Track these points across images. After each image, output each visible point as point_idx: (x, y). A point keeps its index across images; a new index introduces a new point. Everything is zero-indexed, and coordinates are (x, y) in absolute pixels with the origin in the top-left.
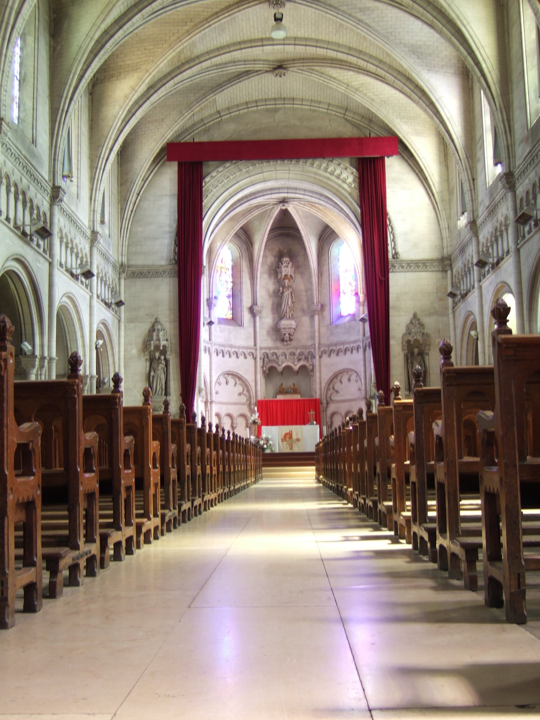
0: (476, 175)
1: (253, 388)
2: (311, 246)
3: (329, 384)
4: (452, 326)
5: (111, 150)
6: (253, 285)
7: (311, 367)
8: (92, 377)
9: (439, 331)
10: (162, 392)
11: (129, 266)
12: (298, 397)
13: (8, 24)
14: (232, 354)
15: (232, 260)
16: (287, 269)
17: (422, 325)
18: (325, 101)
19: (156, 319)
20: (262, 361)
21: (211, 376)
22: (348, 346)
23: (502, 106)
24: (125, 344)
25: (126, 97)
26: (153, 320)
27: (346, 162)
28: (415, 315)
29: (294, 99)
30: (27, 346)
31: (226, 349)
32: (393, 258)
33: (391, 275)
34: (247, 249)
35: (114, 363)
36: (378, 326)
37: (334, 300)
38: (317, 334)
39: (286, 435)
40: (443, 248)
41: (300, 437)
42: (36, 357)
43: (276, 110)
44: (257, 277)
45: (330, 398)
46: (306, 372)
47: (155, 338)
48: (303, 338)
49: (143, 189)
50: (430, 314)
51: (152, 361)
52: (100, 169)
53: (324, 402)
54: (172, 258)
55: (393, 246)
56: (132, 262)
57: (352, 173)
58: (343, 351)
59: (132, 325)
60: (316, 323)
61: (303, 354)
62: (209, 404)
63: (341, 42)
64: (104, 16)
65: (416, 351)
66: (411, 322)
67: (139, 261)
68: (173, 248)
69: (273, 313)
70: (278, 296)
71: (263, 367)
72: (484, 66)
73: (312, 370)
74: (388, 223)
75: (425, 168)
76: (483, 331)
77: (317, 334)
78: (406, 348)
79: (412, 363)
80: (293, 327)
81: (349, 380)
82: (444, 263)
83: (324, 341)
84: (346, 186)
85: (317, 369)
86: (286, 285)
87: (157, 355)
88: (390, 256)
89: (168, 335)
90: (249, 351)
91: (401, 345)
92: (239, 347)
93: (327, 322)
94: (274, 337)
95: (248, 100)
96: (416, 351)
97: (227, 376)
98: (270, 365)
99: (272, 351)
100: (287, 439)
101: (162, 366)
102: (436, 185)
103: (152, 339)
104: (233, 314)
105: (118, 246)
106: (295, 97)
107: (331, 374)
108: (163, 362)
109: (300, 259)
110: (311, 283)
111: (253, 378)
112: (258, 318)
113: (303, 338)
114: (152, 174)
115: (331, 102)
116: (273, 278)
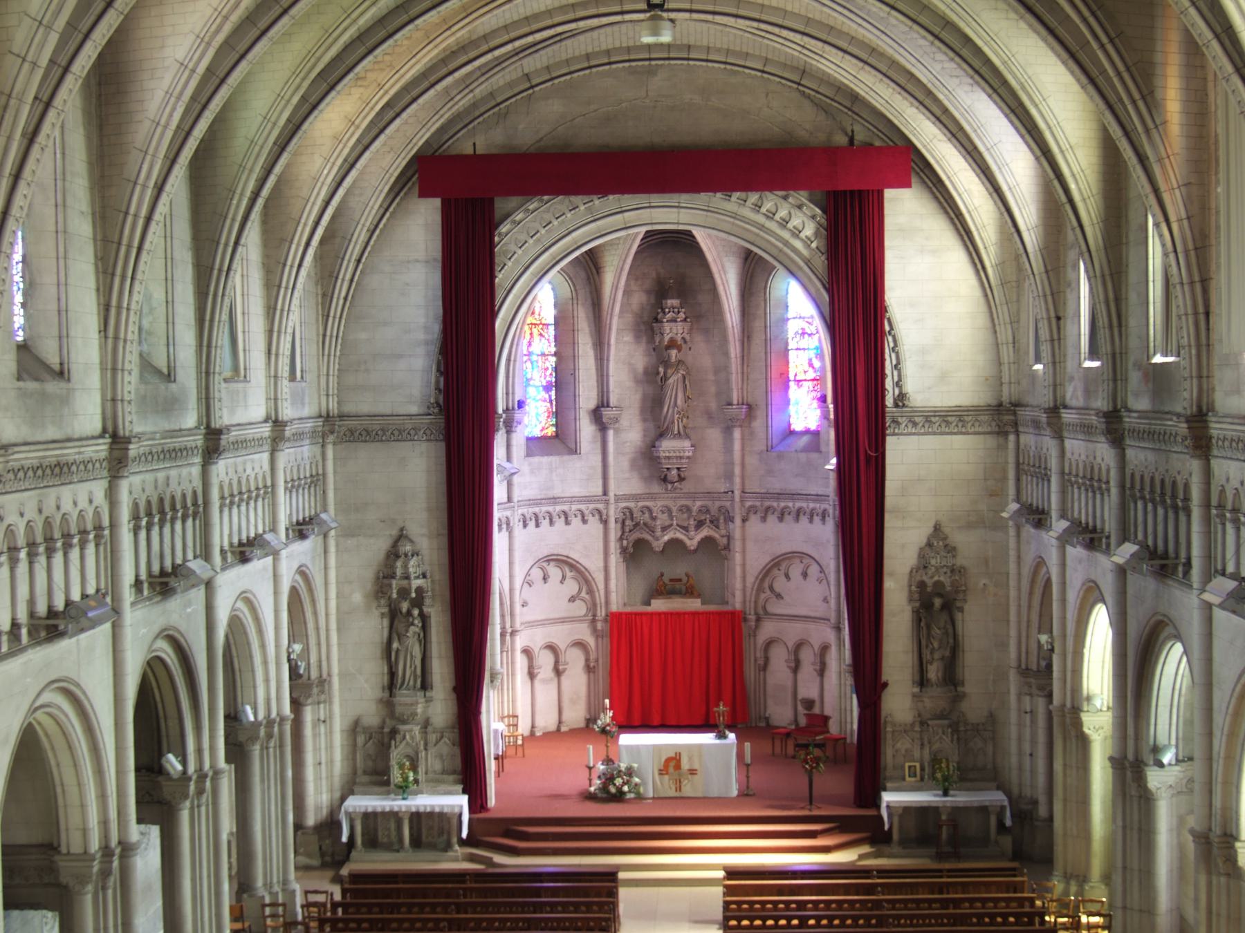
0: (1065, 310)
1: (601, 586)
2: (728, 280)
3: (762, 580)
4: (1012, 553)
5: (308, 244)
6: (602, 359)
7: (725, 541)
8: (282, 719)
9: (986, 562)
10: (415, 681)
11: (342, 416)
12: (694, 605)
13: (129, 246)
14: (555, 518)
15: (556, 306)
16: (673, 329)
17: (951, 550)
18: (757, 53)
19: (402, 530)
20: (619, 525)
21: (511, 576)
22: (804, 505)
23: (1107, 272)
24: (337, 582)
25: (338, 139)
26: (395, 532)
27: (802, 196)
28: (937, 528)
29: (689, 46)
30: (172, 763)
31: (544, 509)
32: (896, 405)
33: (890, 441)
34: (589, 279)
35: (317, 629)
36: (860, 556)
37: (776, 397)
38: (737, 470)
39: (668, 760)
40: (1002, 384)
41: (696, 766)
42: (190, 779)
43: (651, 72)
44: (609, 345)
45: (764, 608)
46: (715, 550)
47: (399, 572)
48: (707, 474)
49: (369, 249)
50: (970, 526)
51: (393, 615)
52: (287, 288)
53: (752, 617)
54: (432, 400)
55: (896, 379)
56: (349, 408)
57: (813, 217)
58: (794, 514)
59: (351, 542)
60: (737, 446)
61: (708, 511)
62: (508, 638)
63: (789, 8)
64: (298, 80)
65: (938, 602)
66: (929, 544)
67: (364, 404)
68: (433, 380)
69: (644, 420)
70: (654, 383)
71: (621, 539)
72: (1073, 186)
73: (727, 547)
74: (887, 328)
75: (969, 212)
76: (1064, 636)
77: (737, 470)
78: (916, 596)
79: (928, 627)
80: (687, 454)
81: (805, 575)
82: (1002, 416)
83: (753, 486)
84: (798, 245)
85: (737, 545)
86: (673, 359)
87: (405, 606)
88: (889, 401)
89: (426, 563)
90: (592, 506)
91: (906, 589)
92: (572, 500)
93: (760, 445)
94: (646, 473)
95: (590, 50)
96: (938, 602)
97: (545, 564)
98: (636, 535)
99: (641, 504)
100: (671, 770)
101: (415, 629)
102: (992, 250)
103: (393, 576)
104: (557, 425)
105: (319, 376)
106: (692, 43)
107: (768, 559)
108: (416, 622)
109: (703, 298)
110: (726, 354)
111: (601, 564)
112: (611, 433)
113: (707, 474)
114: (388, 215)
115: (770, 57)
116: (644, 340)
